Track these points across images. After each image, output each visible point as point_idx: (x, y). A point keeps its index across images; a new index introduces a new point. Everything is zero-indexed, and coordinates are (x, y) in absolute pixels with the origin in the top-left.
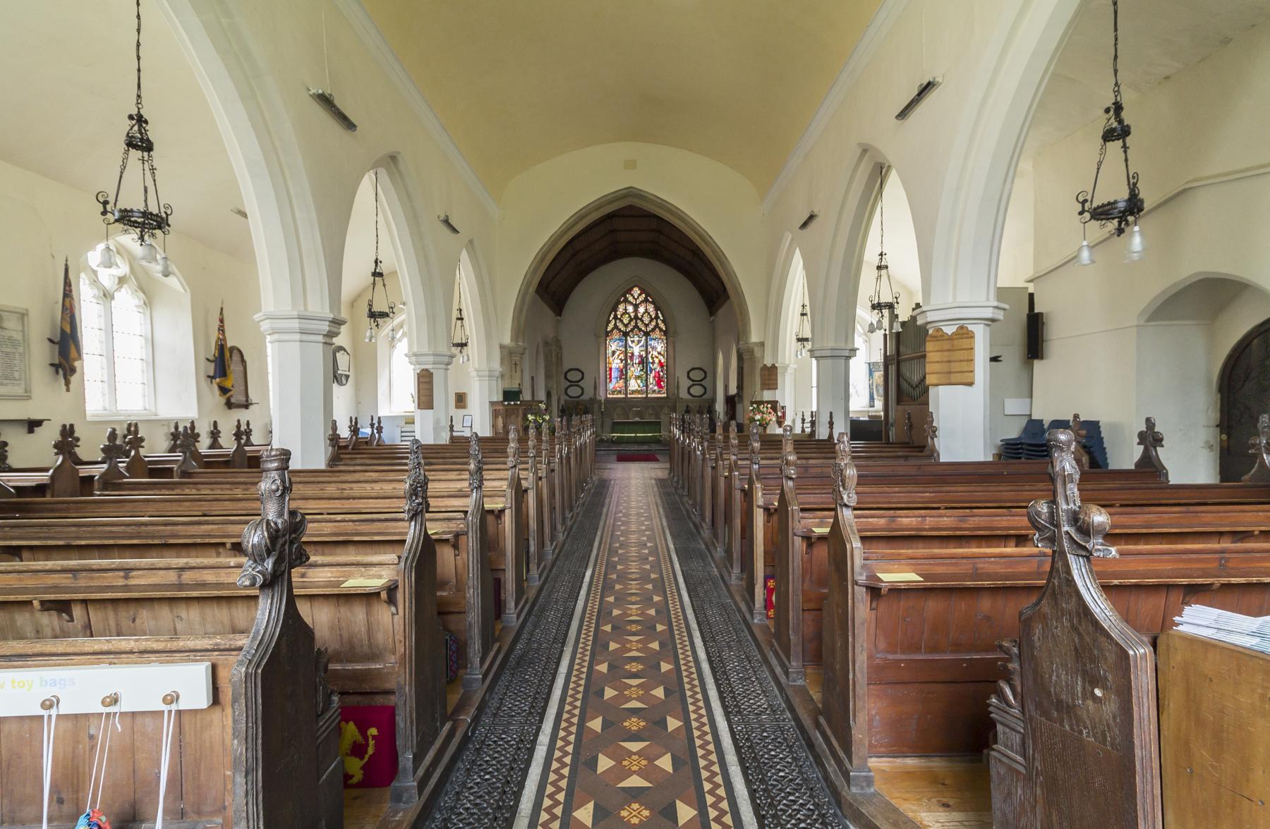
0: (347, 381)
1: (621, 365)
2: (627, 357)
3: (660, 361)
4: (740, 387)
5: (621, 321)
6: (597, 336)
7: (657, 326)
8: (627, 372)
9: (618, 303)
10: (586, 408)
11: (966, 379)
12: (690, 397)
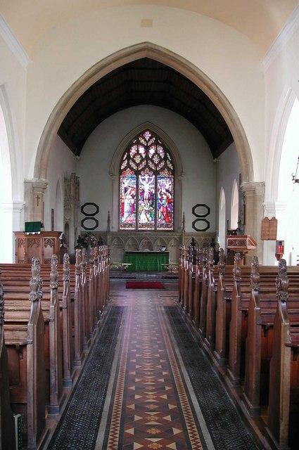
2: (138, 194)
3: (168, 198)
4: (242, 222)
6: (111, 174)
9: (131, 145)
10: (100, 239)
12: (195, 231)
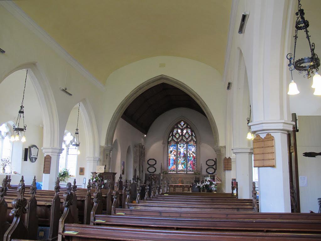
0: (35, 161)
1: (175, 158)
2: (178, 154)
3: (193, 156)
5: (175, 137)
7: (192, 139)
8: (177, 161)
11: (271, 163)
